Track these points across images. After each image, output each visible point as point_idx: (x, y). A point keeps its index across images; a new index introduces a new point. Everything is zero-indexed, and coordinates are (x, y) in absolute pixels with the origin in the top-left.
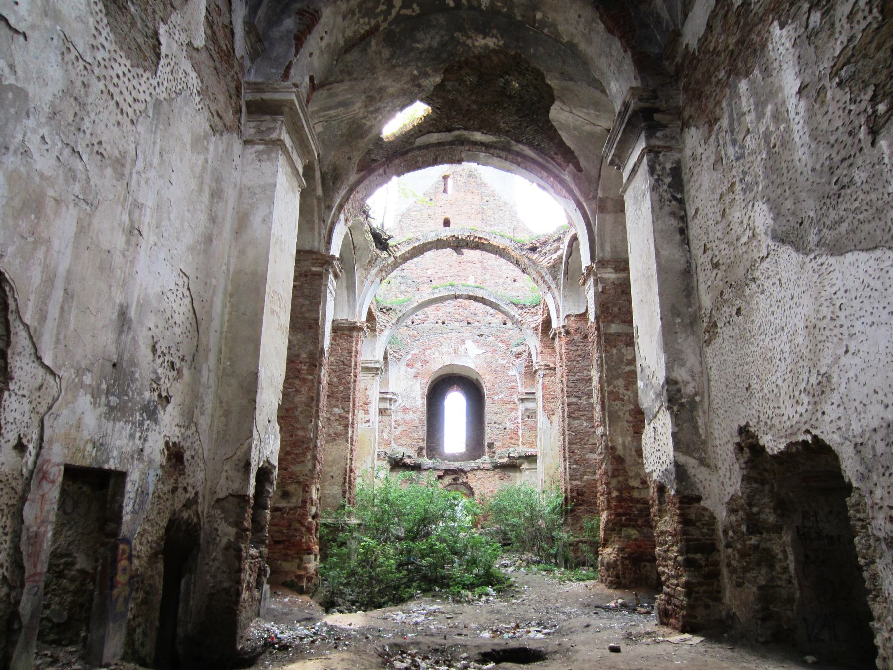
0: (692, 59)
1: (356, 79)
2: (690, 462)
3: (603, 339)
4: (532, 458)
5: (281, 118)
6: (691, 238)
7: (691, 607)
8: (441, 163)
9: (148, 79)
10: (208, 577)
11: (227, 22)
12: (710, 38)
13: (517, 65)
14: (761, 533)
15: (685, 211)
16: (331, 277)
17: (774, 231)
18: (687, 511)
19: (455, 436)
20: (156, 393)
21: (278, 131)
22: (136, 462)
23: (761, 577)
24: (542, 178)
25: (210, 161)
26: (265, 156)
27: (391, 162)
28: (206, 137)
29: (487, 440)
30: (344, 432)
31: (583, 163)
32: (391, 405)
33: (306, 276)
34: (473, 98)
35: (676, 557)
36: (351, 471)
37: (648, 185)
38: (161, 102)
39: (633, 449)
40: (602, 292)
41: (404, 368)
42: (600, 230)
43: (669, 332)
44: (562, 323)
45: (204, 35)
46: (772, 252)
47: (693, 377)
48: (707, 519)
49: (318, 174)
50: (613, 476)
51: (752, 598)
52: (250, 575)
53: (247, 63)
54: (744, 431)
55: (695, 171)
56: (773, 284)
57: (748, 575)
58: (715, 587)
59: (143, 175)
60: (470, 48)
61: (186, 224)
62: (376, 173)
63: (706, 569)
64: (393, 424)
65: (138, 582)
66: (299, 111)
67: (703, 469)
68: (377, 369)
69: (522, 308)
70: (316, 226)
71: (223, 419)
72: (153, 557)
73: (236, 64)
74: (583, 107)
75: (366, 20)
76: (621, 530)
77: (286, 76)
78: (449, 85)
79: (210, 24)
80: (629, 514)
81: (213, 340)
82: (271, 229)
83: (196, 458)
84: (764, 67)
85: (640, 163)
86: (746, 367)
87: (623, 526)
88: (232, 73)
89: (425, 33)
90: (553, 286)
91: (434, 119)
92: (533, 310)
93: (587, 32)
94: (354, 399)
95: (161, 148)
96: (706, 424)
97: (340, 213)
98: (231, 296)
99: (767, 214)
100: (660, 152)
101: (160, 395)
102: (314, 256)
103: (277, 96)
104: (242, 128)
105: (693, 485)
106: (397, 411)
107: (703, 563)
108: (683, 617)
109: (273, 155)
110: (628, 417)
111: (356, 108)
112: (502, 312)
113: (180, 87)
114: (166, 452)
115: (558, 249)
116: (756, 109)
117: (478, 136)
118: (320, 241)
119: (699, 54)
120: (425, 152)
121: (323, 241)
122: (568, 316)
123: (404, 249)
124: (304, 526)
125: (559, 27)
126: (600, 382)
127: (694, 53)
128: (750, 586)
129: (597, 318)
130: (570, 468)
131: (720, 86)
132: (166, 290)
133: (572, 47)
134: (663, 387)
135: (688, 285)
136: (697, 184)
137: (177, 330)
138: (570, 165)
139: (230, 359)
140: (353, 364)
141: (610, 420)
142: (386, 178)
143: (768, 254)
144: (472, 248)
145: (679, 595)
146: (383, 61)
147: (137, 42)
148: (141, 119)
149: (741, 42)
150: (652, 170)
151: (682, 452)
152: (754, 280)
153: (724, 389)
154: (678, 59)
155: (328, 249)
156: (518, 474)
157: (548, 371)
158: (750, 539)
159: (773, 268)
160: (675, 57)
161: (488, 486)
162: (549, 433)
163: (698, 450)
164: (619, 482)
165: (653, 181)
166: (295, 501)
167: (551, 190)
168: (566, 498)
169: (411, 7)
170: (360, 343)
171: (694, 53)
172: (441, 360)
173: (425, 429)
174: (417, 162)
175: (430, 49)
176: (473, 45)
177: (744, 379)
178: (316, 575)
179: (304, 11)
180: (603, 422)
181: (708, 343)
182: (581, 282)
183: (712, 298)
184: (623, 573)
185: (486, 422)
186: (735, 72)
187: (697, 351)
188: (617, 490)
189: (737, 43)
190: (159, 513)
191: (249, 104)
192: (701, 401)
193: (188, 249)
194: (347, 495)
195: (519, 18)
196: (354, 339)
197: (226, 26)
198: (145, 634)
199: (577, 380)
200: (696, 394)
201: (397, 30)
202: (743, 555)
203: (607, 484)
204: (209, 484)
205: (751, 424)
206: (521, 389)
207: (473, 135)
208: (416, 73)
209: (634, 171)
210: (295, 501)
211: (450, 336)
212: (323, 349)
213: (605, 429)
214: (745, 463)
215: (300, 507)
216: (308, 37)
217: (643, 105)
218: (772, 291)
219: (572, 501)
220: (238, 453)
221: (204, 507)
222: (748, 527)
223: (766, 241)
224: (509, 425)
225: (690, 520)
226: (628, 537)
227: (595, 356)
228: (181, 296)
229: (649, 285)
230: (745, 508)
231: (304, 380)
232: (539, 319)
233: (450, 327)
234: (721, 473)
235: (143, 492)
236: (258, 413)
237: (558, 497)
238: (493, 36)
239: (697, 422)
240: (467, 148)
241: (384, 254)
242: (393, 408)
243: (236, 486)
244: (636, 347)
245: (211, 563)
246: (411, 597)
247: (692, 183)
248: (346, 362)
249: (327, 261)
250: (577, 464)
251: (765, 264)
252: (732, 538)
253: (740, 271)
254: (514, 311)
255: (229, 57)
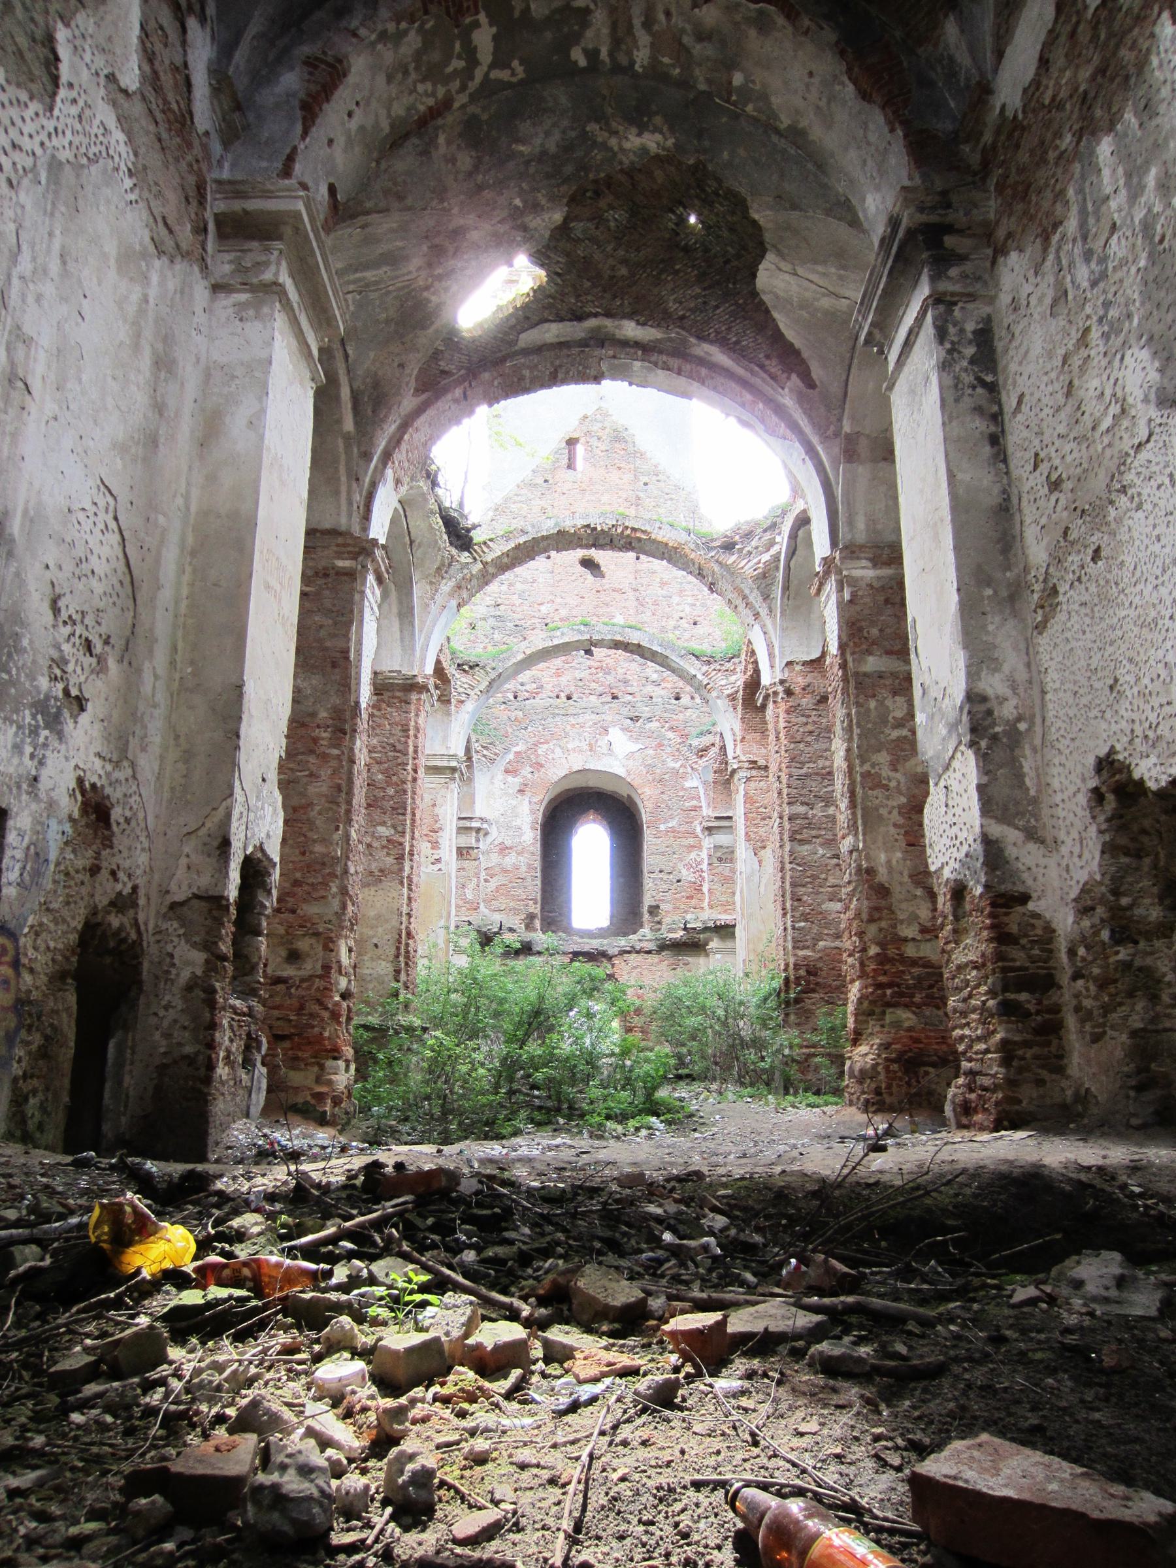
0: (1013, 129)
1: (409, 209)
2: (1010, 835)
3: (852, 684)
4: (725, 931)
5: (278, 245)
6: (1010, 449)
7: (1011, 1083)
8: (564, 381)
9: (37, 114)
10: (157, 1036)
11: (178, 61)
12: (1044, 82)
13: (698, 185)
14: (1136, 943)
15: (1000, 405)
16: (371, 578)
17: (1161, 390)
18: (1006, 919)
19: (591, 897)
20: (60, 686)
21: (273, 268)
22: (24, 797)
23: (1136, 1017)
24: (743, 405)
25: (151, 300)
26: (251, 312)
27: (475, 376)
28: (144, 255)
29: (647, 901)
30: (396, 867)
31: (817, 372)
32: (478, 840)
33: (326, 575)
34: (621, 253)
35: (984, 1003)
36: (409, 935)
37: (934, 362)
38: (60, 163)
39: (906, 873)
40: (851, 601)
41: (500, 776)
42: (846, 493)
43: (972, 613)
44: (779, 676)
45: (137, 72)
46: (1158, 430)
47: (1014, 688)
48: (1039, 932)
49: (345, 393)
50: (871, 920)
51: (1119, 1054)
52: (231, 1041)
53: (216, 148)
54: (1107, 764)
55: (1017, 330)
56: (1159, 487)
57: (1114, 1017)
58: (1053, 1049)
59: (31, 286)
60: (615, 154)
61: (109, 399)
62: (449, 396)
63: (1039, 1018)
64: (483, 873)
65: (30, 1015)
66: (311, 235)
67: (1032, 846)
68: (454, 770)
69: (709, 663)
70: (344, 489)
71: (180, 765)
72: (59, 978)
73: (196, 143)
74: (816, 262)
75: (429, 86)
76: (884, 1013)
77: (287, 172)
78: (578, 228)
79: (149, 56)
80: (898, 986)
81: (160, 625)
82: (262, 438)
83: (133, 823)
84: (1143, 102)
85: (920, 328)
86: (1110, 650)
87: (889, 1005)
88: (189, 158)
89: (534, 125)
90: (763, 612)
91: (550, 296)
92: (729, 666)
93: (823, 103)
94: (413, 810)
95: (63, 247)
96: (1037, 769)
97: (385, 465)
98: (193, 553)
99: (1148, 365)
100: (955, 304)
101: (66, 692)
102: (340, 540)
103: (272, 205)
104: (209, 261)
105: (1014, 875)
106: (488, 852)
107: (1032, 1007)
108: (997, 1104)
109: (266, 310)
110: (895, 817)
111: (411, 268)
112: (673, 671)
113: (94, 149)
114: (79, 798)
115: (772, 543)
116: (1128, 184)
117: (630, 329)
118: (350, 515)
119: (1025, 118)
120: (535, 358)
121: (355, 514)
122: (789, 664)
123: (499, 549)
124: (326, 1009)
125: (773, 99)
126: (847, 758)
127: (1015, 117)
128: (1115, 1034)
129: (842, 647)
130: (794, 928)
131: (1063, 162)
132: (75, 507)
133: (797, 135)
134: (961, 708)
135: (1005, 533)
136: (1022, 351)
137: (99, 587)
138: (794, 376)
139: (192, 663)
140: (411, 749)
141: (865, 824)
142: (466, 406)
143: (1150, 435)
144: (620, 550)
145: (990, 1067)
146: (461, 177)
147: (16, 44)
148: (26, 182)
149: (1101, 71)
150: (941, 334)
151: (996, 818)
152: (1123, 490)
153: (1071, 701)
154: (988, 137)
155: (365, 529)
156: (702, 960)
157: (754, 772)
158: (1117, 953)
159: (1160, 458)
160: (981, 134)
161: (647, 979)
162: (756, 879)
163: (1023, 814)
164: (881, 930)
165: (943, 354)
166: (310, 967)
167: (760, 427)
168: (787, 980)
169: (508, 66)
170: (423, 714)
171: (1015, 117)
172: (566, 762)
173: (539, 882)
174: (522, 378)
175: (542, 156)
176: (622, 149)
177: (1106, 673)
178: (350, 1095)
179: (317, 59)
180: (853, 826)
181: (1041, 627)
182: (813, 591)
183: (1048, 544)
184: (889, 1087)
185: (645, 870)
186: (1089, 129)
187: (1022, 646)
188: (878, 944)
189: (1093, 78)
190: (68, 903)
191: (220, 220)
192: (1028, 730)
193: (114, 445)
194: (403, 977)
195: (702, 87)
196: (413, 707)
197: (177, 69)
198: (43, 1108)
199: (806, 775)
200: (1019, 719)
201: (485, 117)
202: (1103, 983)
203: (861, 934)
204: (156, 877)
205: (1118, 747)
206: (707, 811)
207: (619, 327)
208: (518, 202)
209: (908, 344)
210: (310, 967)
211: (581, 719)
212: (357, 703)
213: (857, 840)
214: (1108, 820)
215: (320, 977)
216: (325, 106)
217: (923, 218)
218: (1156, 500)
219: (798, 984)
220: (208, 825)
221: (148, 914)
222: (1113, 931)
223: (1145, 413)
224: (686, 875)
225: (1009, 935)
226: (897, 1024)
227: (839, 714)
228: (102, 526)
229: (936, 538)
230: (1109, 907)
231: (325, 757)
232: (739, 680)
233: (582, 704)
234: (1064, 850)
235: (37, 854)
236: (242, 757)
237: (773, 979)
238: (657, 130)
239: (1021, 767)
240: (611, 353)
241: (465, 557)
242: (481, 845)
243: (204, 881)
244: (913, 656)
245: (162, 1013)
246: (516, 1133)
247: (1011, 353)
248: (399, 747)
249: (364, 549)
250: (806, 920)
251: (1144, 455)
252: (1084, 959)
253: (1098, 483)
254: (694, 668)
255: (183, 125)
